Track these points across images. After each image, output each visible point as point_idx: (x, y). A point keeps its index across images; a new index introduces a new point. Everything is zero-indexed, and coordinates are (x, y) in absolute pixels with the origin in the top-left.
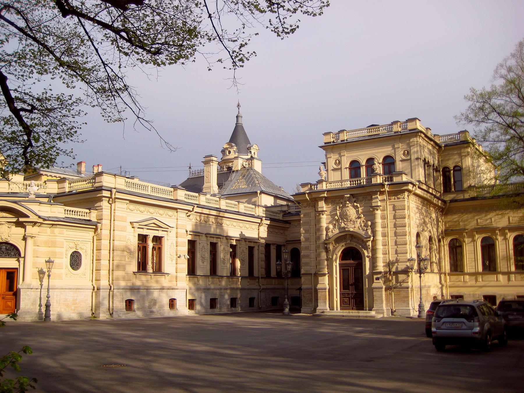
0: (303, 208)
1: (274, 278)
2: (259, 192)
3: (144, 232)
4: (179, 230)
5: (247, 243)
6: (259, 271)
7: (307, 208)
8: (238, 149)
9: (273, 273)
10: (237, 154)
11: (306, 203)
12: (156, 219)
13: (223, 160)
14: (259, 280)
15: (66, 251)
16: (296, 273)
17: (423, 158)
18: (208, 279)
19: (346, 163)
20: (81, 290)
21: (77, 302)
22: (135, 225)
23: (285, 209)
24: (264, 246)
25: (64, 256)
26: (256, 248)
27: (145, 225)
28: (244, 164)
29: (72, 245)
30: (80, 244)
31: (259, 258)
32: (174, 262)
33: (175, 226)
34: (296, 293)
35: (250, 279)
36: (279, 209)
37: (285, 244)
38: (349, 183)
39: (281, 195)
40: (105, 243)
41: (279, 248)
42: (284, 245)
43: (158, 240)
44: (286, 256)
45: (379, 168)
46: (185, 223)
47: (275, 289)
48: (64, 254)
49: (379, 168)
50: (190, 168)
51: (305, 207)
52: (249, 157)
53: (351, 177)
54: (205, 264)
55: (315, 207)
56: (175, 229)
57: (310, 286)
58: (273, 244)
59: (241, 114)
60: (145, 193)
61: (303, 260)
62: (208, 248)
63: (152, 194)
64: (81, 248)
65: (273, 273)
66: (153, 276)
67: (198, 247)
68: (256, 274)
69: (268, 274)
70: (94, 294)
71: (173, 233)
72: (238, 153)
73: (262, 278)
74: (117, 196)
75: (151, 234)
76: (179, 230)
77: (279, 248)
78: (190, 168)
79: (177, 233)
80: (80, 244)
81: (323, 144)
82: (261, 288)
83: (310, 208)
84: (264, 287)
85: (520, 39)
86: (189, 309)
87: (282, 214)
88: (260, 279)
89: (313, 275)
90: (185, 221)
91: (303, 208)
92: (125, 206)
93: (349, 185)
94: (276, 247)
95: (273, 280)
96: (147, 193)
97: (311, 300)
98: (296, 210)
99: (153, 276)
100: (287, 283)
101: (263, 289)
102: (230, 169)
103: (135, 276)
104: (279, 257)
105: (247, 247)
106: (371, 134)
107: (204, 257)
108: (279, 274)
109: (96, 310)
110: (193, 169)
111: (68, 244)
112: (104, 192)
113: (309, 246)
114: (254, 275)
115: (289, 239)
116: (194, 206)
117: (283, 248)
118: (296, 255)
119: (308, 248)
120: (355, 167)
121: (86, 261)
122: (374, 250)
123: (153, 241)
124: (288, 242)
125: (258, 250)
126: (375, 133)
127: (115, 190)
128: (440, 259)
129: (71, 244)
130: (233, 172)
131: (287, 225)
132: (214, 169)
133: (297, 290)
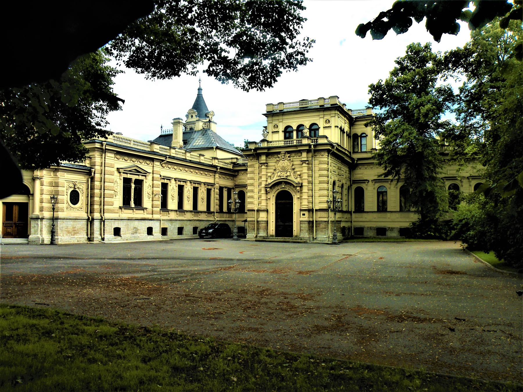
1: (226, 213)
2: (215, 147)
3: (129, 176)
4: (155, 175)
5: (206, 186)
7: (253, 161)
8: (198, 114)
9: (225, 209)
10: (198, 118)
12: (137, 166)
15: (67, 189)
16: (241, 209)
17: (339, 127)
18: (176, 213)
19: (281, 128)
20: (79, 220)
21: (76, 229)
22: (121, 170)
23: (235, 161)
25: (65, 194)
26: (213, 190)
27: (129, 171)
28: (204, 126)
29: (72, 186)
30: (78, 185)
32: (151, 199)
33: (150, 171)
34: (242, 224)
36: (230, 161)
38: (283, 142)
40: (97, 184)
41: (229, 190)
43: (139, 183)
44: (235, 196)
45: (306, 132)
46: (159, 170)
48: (65, 192)
49: (306, 132)
50: (162, 127)
52: (208, 120)
53: (285, 138)
56: (151, 174)
58: (226, 187)
59: (202, 87)
60: (128, 145)
61: (248, 200)
62: (177, 189)
63: (134, 147)
64: (78, 188)
65: (225, 209)
66: (134, 210)
67: (170, 188)
69: (221, 211)
70: (89, 223)
71: (150, 177)
72: (199, 117)
73: (217, 212)
74: (107, 148)
75: (134, 177)
76: (155, 175)
77: (229, 190)
78: (162, 127)
79: (153, 177)
80: (78, 185)
81: (265, 112)
84: (218, 219)
86: (162, 235)
87: (232, 165)
92: (113, 155)
93: (283, 145)
95: (225, 215)
96: (130, 146)
97: (254, 229)
98: (243, 162)
99: (134, 210)
100: (235, 217)
102: (191, 129)
103: (120, 210)
104: (229, 197)
106: (302, 106)
108: (229, 211)
109: (91, 235)
111: (68, 184)
112: (96, 144)
115: (237, 184)
116: (166, 157)
117: (232, 190)
118: (242, 196)
120: (288, 131)
121: (82, 198)
122: (150, 275)
123: (135, 184)
124: (237, 186)
125: (214, 191)
126: (305, 106)
127: (105, 143)
128: (249, 329)
129: (70, 184)
130: (195, 131)
132: (181, 129)
133: (242, 221)
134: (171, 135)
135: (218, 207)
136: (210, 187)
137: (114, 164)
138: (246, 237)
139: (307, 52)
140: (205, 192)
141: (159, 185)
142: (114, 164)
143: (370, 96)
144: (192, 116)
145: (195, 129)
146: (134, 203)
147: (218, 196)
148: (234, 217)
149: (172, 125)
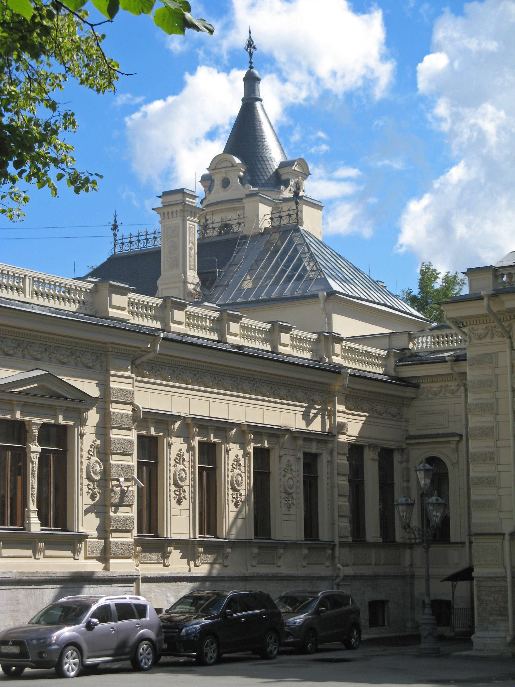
0: (474, 341)
1: (374, 545)
6: (333, 524)
7: (487, 340)
11: (484, 326)
13: (207, 206)
14: (333, 549)
24: (347, 451)
31: (332, 487)
35: (309, 548)
37: (404, 446)
39: (385, 305)
42: (402, 450)
46: (129, 387)
47: (375, 577)
50: (115, 227)
51: (480, 338)
54: (293, 510)
55: (510, 338)
57: (498, 571)
58: (370, 446)
68: (399, 535)
78: (115, 227)
82: (341, 575)
83: (496, 339)
84: (349, 571)
85: (344, 5)
88: (337, 549)
89: (507, 537)
90: (131, 381)
91: (474, 341)
94: (380, 455)
96: (21, 298)
101: (346, 578)
105: (300, 455)
107: (290, 491)
110: (123, 231)
113: (493, 453)
114: (321, 537)
115: (413, 431)
119: (492, 459)
125: (330, 462)
131: (409, 392)
134: (156, 254)
135: (345, 524)
136: (313, 449)
137: (132, 393)
138: (469, 642)
139: (117, 78)
140: (299, 468)
141: (131, 442)
142: (132, 393)
143: (207, 172)
144: (226, 183)
145: (247, 230)
146: (40, 516)
147: (344, 482)
148: (408, 563)
149: (158, 218)
